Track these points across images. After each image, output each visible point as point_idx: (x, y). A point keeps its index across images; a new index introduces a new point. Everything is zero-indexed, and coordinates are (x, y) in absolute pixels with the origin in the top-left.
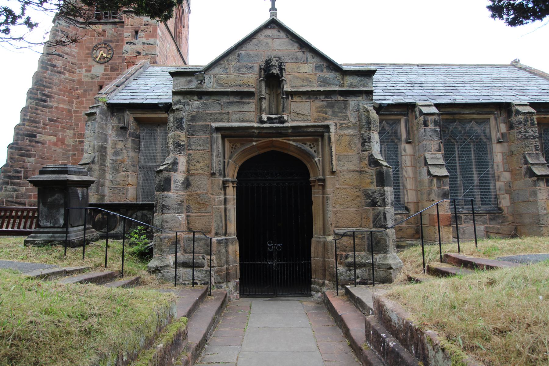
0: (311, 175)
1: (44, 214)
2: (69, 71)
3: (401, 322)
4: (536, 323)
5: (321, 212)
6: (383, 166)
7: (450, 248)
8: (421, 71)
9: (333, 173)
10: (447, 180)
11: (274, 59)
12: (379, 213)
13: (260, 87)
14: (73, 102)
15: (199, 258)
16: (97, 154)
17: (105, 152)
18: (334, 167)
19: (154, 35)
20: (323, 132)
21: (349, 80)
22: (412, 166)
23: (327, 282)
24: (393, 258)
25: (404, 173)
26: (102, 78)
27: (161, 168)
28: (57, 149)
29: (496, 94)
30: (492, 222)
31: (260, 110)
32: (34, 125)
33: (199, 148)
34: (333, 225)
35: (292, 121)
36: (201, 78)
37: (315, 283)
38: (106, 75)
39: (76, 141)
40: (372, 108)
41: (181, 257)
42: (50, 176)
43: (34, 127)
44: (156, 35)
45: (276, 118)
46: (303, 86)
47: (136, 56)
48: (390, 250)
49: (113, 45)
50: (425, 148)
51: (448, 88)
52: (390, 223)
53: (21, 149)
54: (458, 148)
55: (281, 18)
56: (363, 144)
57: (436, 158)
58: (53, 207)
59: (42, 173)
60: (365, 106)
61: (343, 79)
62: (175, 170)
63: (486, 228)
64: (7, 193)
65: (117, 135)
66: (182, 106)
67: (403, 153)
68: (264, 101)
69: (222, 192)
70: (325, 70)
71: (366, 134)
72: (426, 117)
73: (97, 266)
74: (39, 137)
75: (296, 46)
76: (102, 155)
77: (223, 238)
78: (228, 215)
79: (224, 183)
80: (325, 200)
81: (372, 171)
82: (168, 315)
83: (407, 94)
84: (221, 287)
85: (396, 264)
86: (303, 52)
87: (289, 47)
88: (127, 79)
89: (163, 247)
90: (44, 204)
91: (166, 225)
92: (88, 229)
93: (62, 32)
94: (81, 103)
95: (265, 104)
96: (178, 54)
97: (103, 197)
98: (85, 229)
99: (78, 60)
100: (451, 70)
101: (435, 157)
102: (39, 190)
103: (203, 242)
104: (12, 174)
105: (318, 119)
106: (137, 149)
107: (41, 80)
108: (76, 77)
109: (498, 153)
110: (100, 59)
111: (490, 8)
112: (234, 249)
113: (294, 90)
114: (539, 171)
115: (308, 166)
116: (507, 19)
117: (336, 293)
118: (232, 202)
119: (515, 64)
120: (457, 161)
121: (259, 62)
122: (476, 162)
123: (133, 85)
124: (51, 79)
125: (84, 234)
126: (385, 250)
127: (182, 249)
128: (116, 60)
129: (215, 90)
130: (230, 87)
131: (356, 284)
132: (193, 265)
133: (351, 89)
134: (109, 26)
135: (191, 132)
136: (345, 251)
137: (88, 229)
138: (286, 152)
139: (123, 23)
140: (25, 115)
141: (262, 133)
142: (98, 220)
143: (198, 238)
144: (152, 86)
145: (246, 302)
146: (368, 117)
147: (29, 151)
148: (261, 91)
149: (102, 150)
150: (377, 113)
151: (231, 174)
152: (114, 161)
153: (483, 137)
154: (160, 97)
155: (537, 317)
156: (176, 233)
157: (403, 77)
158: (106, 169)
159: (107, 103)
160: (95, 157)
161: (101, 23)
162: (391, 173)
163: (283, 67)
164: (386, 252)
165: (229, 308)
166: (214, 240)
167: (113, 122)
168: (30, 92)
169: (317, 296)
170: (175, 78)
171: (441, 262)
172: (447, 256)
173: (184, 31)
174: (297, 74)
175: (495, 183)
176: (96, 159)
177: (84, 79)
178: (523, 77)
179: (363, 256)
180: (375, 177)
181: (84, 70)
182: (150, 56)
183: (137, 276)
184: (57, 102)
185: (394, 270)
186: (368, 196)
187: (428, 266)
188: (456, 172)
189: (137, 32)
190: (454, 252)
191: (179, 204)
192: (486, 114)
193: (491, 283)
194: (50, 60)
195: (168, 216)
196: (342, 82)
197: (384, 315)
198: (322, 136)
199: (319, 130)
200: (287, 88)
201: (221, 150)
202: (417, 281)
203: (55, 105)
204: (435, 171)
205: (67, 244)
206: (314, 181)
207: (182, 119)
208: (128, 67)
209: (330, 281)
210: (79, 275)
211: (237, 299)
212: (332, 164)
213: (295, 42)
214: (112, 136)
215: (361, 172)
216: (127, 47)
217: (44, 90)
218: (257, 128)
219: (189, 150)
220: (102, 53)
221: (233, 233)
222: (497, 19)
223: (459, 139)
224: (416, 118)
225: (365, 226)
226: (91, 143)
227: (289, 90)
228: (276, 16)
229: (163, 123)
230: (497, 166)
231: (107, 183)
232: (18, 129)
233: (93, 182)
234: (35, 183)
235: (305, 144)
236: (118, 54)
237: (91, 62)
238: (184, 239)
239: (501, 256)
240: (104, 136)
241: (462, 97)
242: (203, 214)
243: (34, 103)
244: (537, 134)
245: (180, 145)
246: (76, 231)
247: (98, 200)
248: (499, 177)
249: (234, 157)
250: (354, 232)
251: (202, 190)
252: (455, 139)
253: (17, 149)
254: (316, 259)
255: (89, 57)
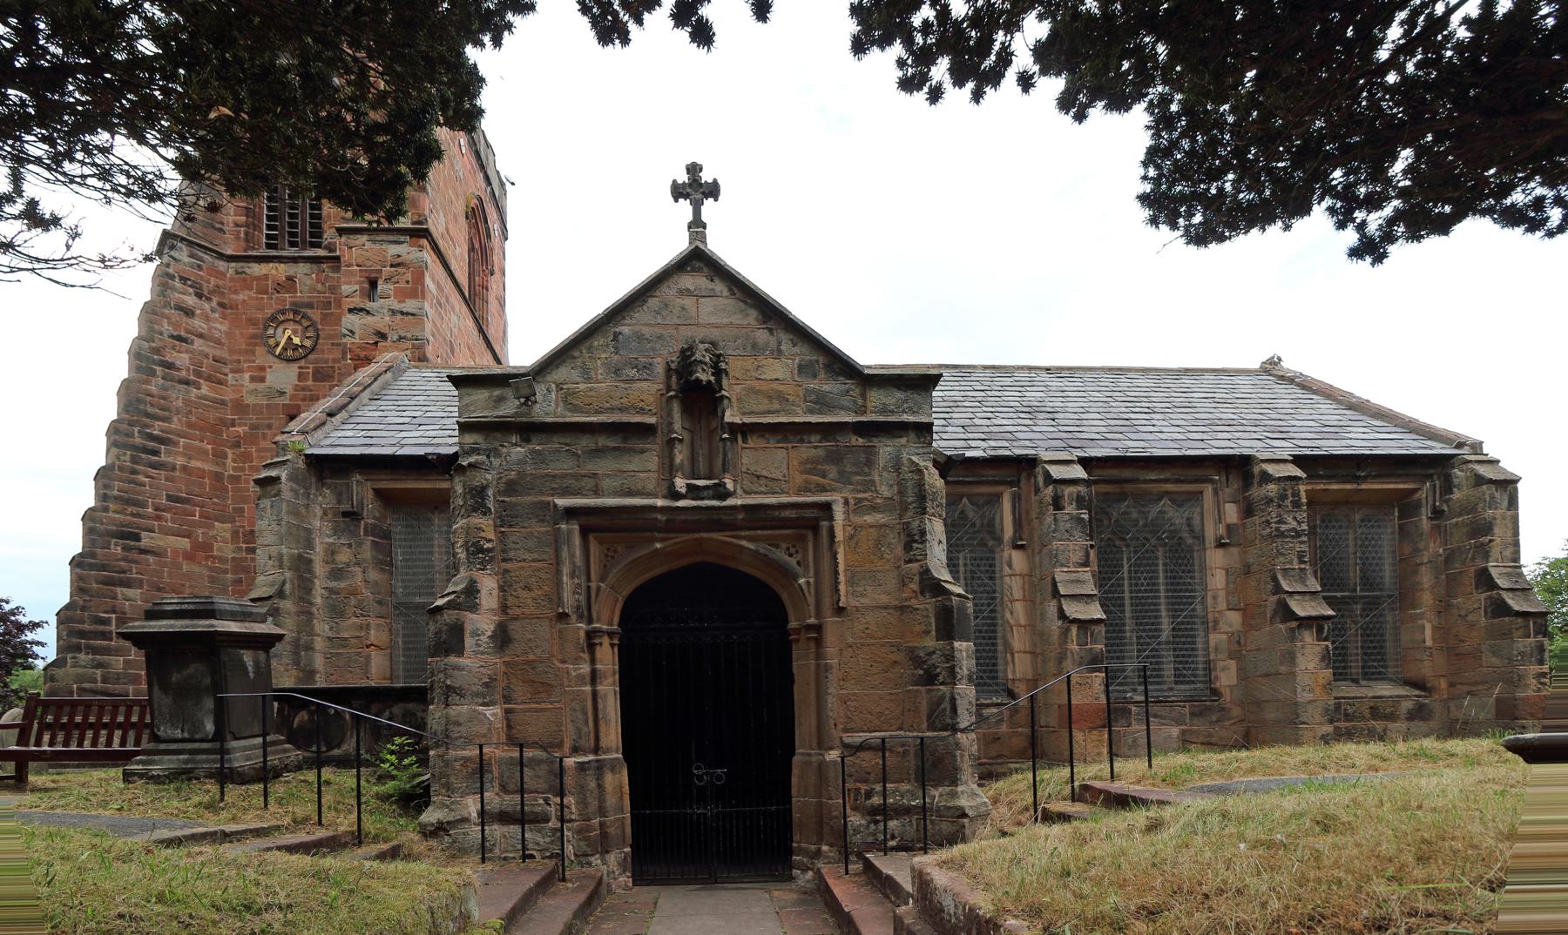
0: (791, 616)
1: (165, 710)
2: (209, 379)
3: (960, 911)
4: (1220, 892)
5: (812, 697)
6: (952, 594)
7: (1092, 772)
8: (1055, 383)
9: (840, 611)
10: (1102, 628)
11: (701, 346)
12: (942, 698)
13: (670, 414)
14: (225, 456)
15: (536, 803)
16: (288, 575)
17: (310, 571)
18: (843, 598)
19: (416, 289)
20: (817, 519)
21: (876, 397)
22: (1024, 599)
23: (825, 848)
24: (970, 795)
25: (1008, 615)
26: (293, 397)
27: (440, 602)
28: (196, 569)
29: (1220, 435)
30: (1196, 721)
31: (669, 469)
32: (134, 509)
33: (527, 556)
34: (840, 727)
35: (746, 492)
36: (525, 391)
37: (800, 851)
38: (303, 389)
39: (240, 549)
40: (930, 465)
41: (494, 799)
42: (172, 622)
43: (132, 514)
44: (423, 292)
45: (706, 488)
46: (770, 412)
47: (376, 343)
48: (964, 778)
49: (315, 315)
50: (1055, 560)
51: (1113, 422)
52: (965, 720)
53: (103, 568)
54: (1129, 559)
55: (718, 245)
56: (908, 547)
57: (1078, 581)
58: (185, 694)
59: (151, 615)
60: (914, 458)
61: (863, 396)
62: (474, 608)
63: (1183, 732)
64: (80, 670)
65: (336, 532)
66: (484, 458)
67: (1007, 570)
68: (678, 447)
69: (586, 656)
70: (822, 375)
71: (915, 524)
72: (1060, 488)
73: (298, 823)
74: (146, 540)
75: (753, 314)
76: (300, 578)
77: (591, 757)
78: (600, 706)
79: (590, 635)
80: (822, 671)
81: (927, 606)
82: (457, 913)
83: (1019, 435)
84: (589, 864)
85: (977, 807)
86: (771, 330)
87: (737, 319)
88: (352, 399)
89: (452, 779)
90: (165, 688)
91: (456, 732)
92: (274, 743)
93: (184, 279)
94: (246, 457)
95: (680, 456)
96: (481, 341)
97: (311, 674)
98: (265, 745)
99: (231, 352)
100: (1124, 382)
101: (1076, 578)
102: (147, 656)
103: (544, 767)
104: (87, 627)
105: (804, 489)
106: (385, 561)
107: (139, 401)
108: (229, 395)
109: (1217, 567)
110: (285, 349)
111: (1144, 199)
112: (618, 781)
113: (747, 420)
114: (1301, 608)
115: (785, 596)
116: (1187, 228)
117: (843, 871)
118: (610, 680)
119: (1271, 368)
120: (1126, 588)
121: (664, 356)
122: (1167, 591)
123: (370, 413)
124: (164, 398)
125: (265, 756)
126: (951, 778)
127: (496, 784)
128: (327, 354)
129: (561, 420)
130: (597, 412)
131: (886, 850)
132: (521, 819)
133: (882, 419)
134: (302, 269)
135: (506, 518)
136: (866, 781)
137: (274, 743)
138: (732, 565)
139: (338, 259)
140: (106, 487)
141: (675, 522)
142: (301, 727)
143: (532, 760)
144: (413, 416)
145: (646, 893)
146: (920, 485)
147: (124, 572)
148: (671, 424)
149: (302, 566)
150: (942, 476)
151: (605, 615)
152: (330, 590)
153: (1185, 535)
154: (435, 441)
155: (1225, 882)
156: (481, 747)
157: (1012, 397)
158: (314, 610)
159: (307, 456)
160: (284, 583)
161: (280, 259)
162: (970, 611)
163: (723, 365)
164: (954, 782)
165: (607, 909)
166: (570, 762)
167: (324, 499)
168: (114, 430)
169: (805, 878)
170: (464, 391)
171: (1073, 801)
172: (1085, 788)
173: (493, 283)
174: (756, 384)
175: (1207, 636)
176: (288, 586)
177: (250, 400)
178: (1286, 396)
179: (903, 792)
180: (933, 620)
181: (247, 376)
182: (409, 344)
183: (395, 843)
184: (185, 455)
185: (971, 820)
186: (917, 661)
187: (1044, 809)
188: (1123, 612)
189: (373, 284)
190: (1101, 779)
191: (486, 685)
192: (1196, 481)
193: (1154, 826)
194: (157, 351)
195: (460, 710)
196: (860, 401)
197: (931, 901)
198: (815, 529)
199: (809, 513)
200: (731, 416)
201: (579, 561)
202: (1012, 835)
203: (180, 461)
204: (1074, 610)
205: (225, 777)
206: (797, 631)
207: (484, 488)
208: (356, 368)
209: (831, 845)
210: (258, 841)
211: (626, 888)
212: (837, 591)
213: (751, 306)
214: (323, 536)
215: (902, 609)
216: (350, 320)
217: (148, 426)
218: (663, 509)
219: (504, 560)
220: (286, 334)
221: (614, 746)
222: (1164, 228)
223: (1132, 539)
224: (1037, 491)
225: (911, 728)
226: (274, 550)
227: (737, 420)
228: (704, 242)
229: (440, 502)
230: (1214, 598)
231: (319, 644)
232: (92, 519)
233: (280, 637)
234: (138, 639)
235: (777, 546)
236: (330, 337)
237: (261, 357)
238: (500, 762)
239: (1199, 784)
240: (302, 534)
241: (1142, 444)
242: (543, 706)
243: (127, 458)
244: (1304, 527)
245: (482, 550)
246: (245, 749)
247: (299, 680)
248: (1216, 622)
249: (611, 577)
250: (883, 740)
251: (538, 652)
252: (1123, 539)
253: (92, 567)
254: (801, 800)
255: (256, 345)
